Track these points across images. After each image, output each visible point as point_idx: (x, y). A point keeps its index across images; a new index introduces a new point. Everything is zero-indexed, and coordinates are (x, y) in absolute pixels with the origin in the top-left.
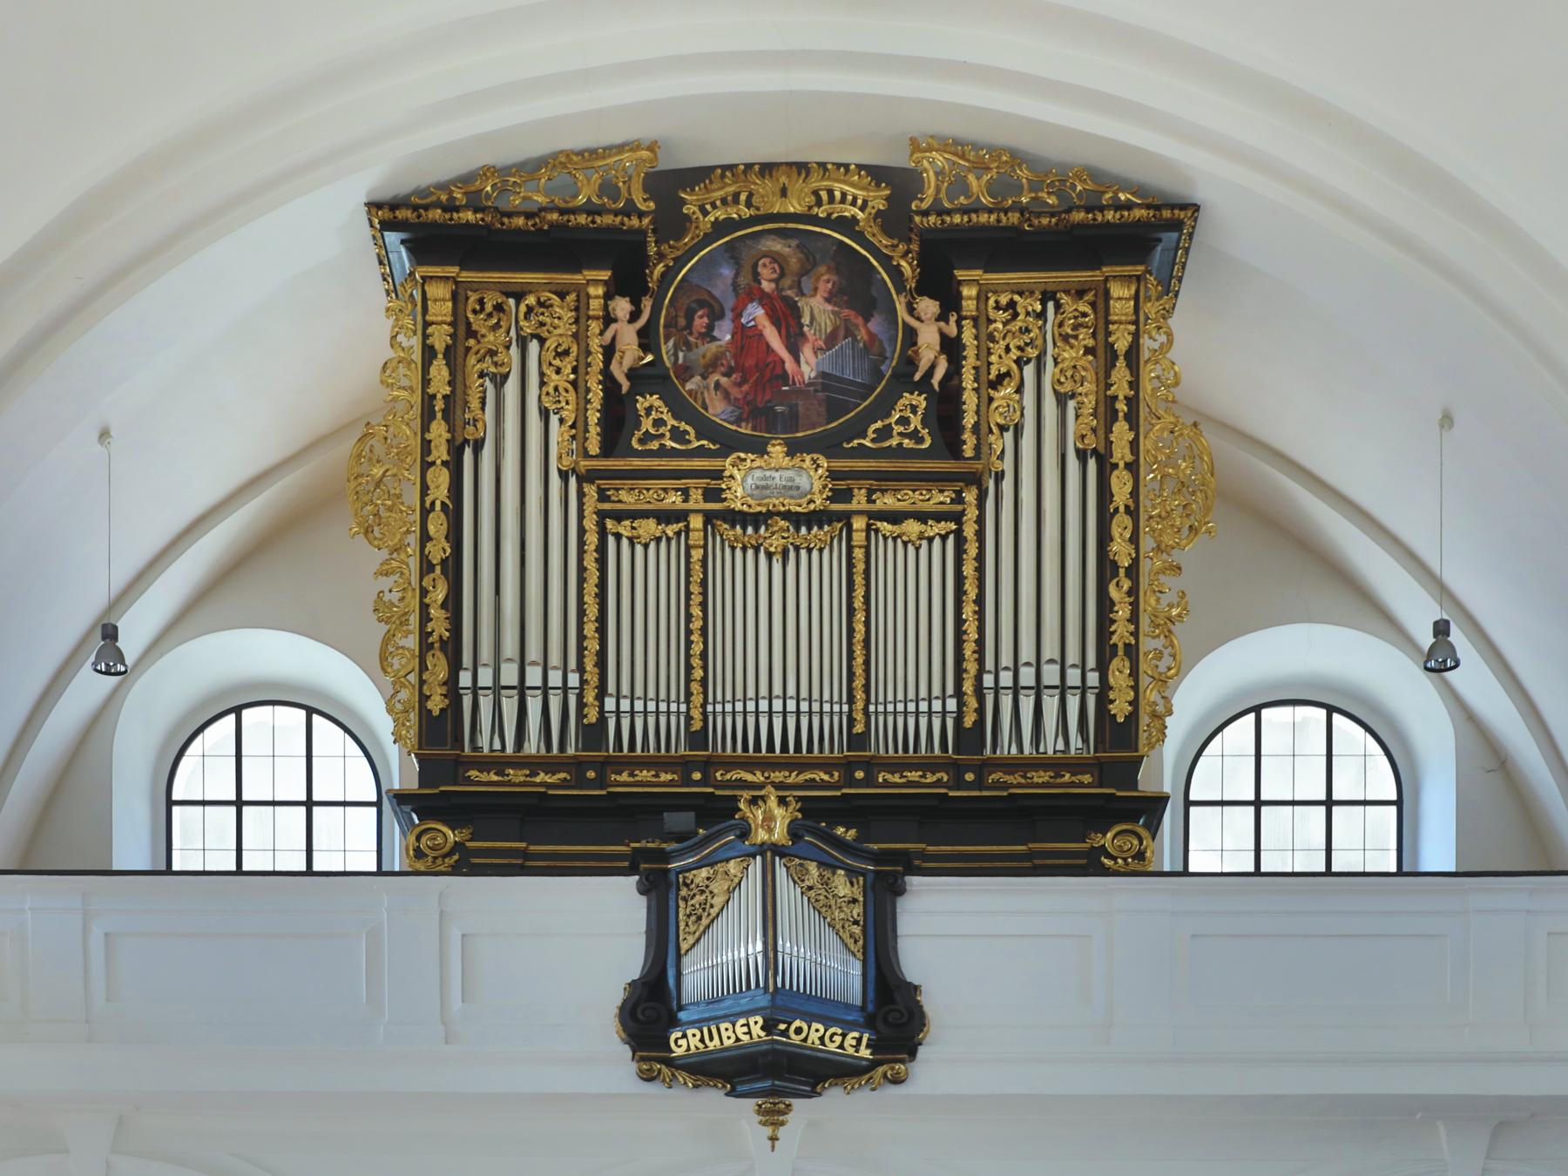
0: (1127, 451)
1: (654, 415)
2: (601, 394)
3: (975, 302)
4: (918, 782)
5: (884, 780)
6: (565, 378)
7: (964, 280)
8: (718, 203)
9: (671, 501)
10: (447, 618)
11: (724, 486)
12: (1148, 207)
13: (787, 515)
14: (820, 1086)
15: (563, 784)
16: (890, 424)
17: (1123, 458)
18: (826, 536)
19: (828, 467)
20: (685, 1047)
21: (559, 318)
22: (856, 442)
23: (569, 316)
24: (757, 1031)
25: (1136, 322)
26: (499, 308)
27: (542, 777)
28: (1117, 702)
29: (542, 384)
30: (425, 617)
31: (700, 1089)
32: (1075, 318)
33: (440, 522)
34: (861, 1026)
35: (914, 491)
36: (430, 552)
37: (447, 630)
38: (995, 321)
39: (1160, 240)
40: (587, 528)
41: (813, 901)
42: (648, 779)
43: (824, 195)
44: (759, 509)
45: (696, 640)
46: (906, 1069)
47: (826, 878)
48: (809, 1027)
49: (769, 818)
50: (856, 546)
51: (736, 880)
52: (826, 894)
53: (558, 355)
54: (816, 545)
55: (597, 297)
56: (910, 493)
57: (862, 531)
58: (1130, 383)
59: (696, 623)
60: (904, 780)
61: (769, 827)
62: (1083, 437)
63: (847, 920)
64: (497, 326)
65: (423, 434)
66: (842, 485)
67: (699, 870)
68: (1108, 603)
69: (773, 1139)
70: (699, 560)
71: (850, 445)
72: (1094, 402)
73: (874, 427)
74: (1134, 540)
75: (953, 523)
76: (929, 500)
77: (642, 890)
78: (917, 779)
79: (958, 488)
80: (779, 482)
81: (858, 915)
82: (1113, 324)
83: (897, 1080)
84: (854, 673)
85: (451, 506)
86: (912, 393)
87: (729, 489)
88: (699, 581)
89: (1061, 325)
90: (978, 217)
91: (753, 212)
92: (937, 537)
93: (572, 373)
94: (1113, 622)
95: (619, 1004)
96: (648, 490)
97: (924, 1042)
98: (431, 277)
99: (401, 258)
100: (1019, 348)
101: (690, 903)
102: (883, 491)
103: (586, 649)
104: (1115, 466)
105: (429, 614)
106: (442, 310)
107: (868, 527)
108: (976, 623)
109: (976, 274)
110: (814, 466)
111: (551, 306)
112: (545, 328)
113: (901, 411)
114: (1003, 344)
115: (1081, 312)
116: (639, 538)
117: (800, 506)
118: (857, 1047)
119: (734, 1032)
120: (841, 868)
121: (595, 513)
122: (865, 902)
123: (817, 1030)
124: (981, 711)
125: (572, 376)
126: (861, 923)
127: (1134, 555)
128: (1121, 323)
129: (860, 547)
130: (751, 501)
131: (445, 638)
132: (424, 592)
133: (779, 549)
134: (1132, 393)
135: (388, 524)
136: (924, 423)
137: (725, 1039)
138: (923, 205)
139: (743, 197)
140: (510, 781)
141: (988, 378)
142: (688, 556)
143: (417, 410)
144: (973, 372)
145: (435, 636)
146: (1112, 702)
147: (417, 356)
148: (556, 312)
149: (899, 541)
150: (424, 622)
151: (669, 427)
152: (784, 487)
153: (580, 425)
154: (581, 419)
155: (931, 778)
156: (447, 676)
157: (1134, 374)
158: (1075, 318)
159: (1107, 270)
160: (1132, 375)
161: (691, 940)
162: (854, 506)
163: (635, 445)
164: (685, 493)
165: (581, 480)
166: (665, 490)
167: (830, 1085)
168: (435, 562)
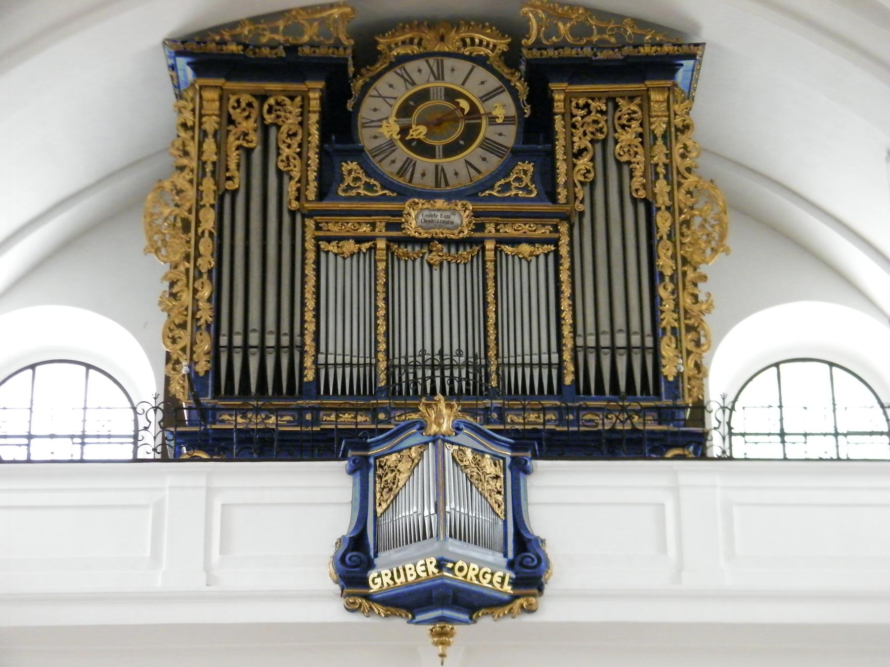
0: (666, 198)
1: (353, 175)
2: (317, 160)
3: (563, 104)
5: (512, 421)
7: (555, 90)
8: (400, 44)
10: (211, 309)
11: (403, 220)
13: (442, 241)
17: (664, 203)
18: (468, 255)
19: (473, 208)
20: (379, 585)
21: (290, 113)
24: (432, 569)
25: (669, 116)
26: (250, 105)
28: (668, 367)
29: (279, 154)
31: (389, 617)
32: (629, 114)
37: (210, 317)
38: (576, 116)
39: (682, 65)
40: (307, 248)
41: (469, 476)
42: (349, 420)
43: (468, 41)
44: (425, 236)
45: (381, 323)
46: (537, 602)
48: (468, 567)
49: (439, 415)
50: (488, 260)
51: (416, 461)
53: (289, 136)
55: (315, 99)
56: (523, 225)
58: (667, 155)
59: (381, 312)
61: (439, 423)
62: (637, 190)
66: (480, 220)
67: (390, 456)
69: (442, 656)
71: (483, 195)
72: (643, 168)
73: (499, 183)
74: (674, 257)
75: (552, 246)
76: (535, 231)
77: (351, 472)
81: (501, 487)
84: (489, 346)
86: (524, 162)
89: (620, 118)
91: (422, 50)
92: (542, 254)
94: (662, 312)
96: (348, 223)
98: (206, 86)
100: (592, 133)
101: (384, 479)
103: (306, 329)
105: (198, 306)
106: (213, 107)
107: (496, 249)
109: (564, 85)
111: (285, 105)
112: (281, 119)
113: (517, 173)
114: (582, 130)
115: (632, 111)
116: (343, 254)
118: (502, 583)
119: (416, 571)
120: (488, 453)
121: (313, 238)
122: (505, 479)
123: (474, 569)
124: (576, 373)
125: (298, 150)
126: (503, 493)
127: (674, 268)
128: (658, 116)
129: (491, 261)
130: (421, 231)
131: (209, 322)
132: (195, 291)
134: (668, 161)
135: (171, 247)
136: (533, 180)
138: (529, 41)
139: (416, 41)
141: (572, 152)
142: (376, 267)
145: (202, 321)
146: (664, 366)
151: (363, 182)
152: (443, 222)
153: (304, 180)
154: (304, 176)
158: (629, 114)
159: (648, 83)
161: (384, 506)
162: (486, 234)
164: (373, 225)
165: (304, 216)
166: (359, 223)
167: (483, 614)
168: (203, 271)
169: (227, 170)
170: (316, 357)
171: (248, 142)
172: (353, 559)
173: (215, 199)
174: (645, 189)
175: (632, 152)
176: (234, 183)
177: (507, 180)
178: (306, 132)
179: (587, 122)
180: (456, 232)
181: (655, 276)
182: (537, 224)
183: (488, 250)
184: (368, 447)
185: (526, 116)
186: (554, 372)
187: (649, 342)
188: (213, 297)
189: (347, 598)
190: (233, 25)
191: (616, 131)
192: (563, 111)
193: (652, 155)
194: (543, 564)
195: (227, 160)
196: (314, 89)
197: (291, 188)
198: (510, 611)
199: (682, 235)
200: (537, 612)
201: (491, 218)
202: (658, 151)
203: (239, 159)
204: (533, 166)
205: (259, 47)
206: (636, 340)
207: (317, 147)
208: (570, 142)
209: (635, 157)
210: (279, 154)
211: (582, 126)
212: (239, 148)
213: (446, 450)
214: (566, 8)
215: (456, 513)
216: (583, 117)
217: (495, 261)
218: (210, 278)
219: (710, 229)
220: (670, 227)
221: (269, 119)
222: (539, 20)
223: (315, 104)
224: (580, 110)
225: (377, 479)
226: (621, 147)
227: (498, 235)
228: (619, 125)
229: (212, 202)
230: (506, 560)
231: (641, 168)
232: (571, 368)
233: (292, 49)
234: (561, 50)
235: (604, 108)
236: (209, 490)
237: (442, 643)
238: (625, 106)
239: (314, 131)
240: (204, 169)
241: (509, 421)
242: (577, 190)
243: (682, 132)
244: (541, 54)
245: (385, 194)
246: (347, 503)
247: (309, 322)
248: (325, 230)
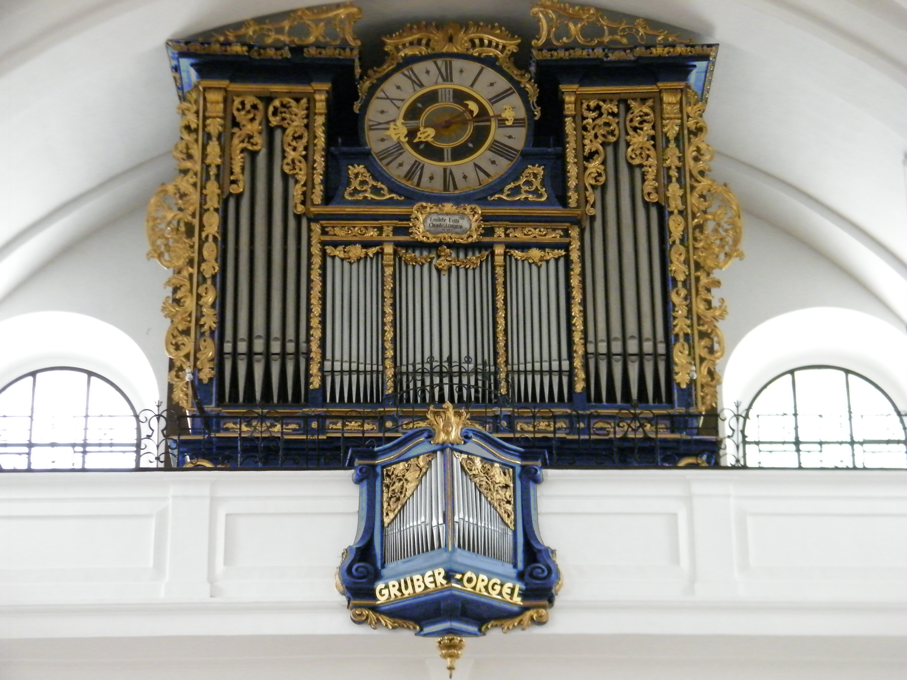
0: (679, 202)
1: (360, 178)
2: (323, 164)
3: (573, 106)
5: (522, 429)
7: (566, 92)
8: (407, 45)
10: (215, 315)
11: (411, 224)
13: (450, 246)
17: (676, 207)
18: (477, 260)
19: (482, 213)
20: (387, 596)
21: (296, 115)
24: (440, 580)
25: (682, 119)
26: (254, 107)
28: (680, 374)
29: (284, 157)
31: (397, 630)
32: (641, 116)
33: (211, 250)
37: (214, 323)
38: (587, 118)
39: (695, 66)
40: (313, 253)
41: (478, 485)
42: (356, 428)
43: (477, 41)
44: (434, 240)
45: (388, 330)
47: (487, 469)
49: (448, 424)
50: (497, 265)
51: (424, 470)
53: (295, 138)
54: (470, 266)
55: (321, 101)
56: (533, 230)
58: (679, 158)
59: (388, 318)
61: (448, 431)
62: (649, 194)
63: (502, 500)
66: (489, 224)
69: (451, 668)
70: (390, 275)
71: (493, 198)
72: (655, 171)
74: (687, 262)
75: (563, 251)
76: (545, 235)
77: (358, 481)
80: (448, 223)
81: (510, 496)
84: (498, 353)
86: (534, 165)
89: (631, 120)
91: (430, 51)
94: (675, 318)
96: (354, 227)
98: (210, 88)
100: (604, 136)
101: (391, 489)
103: (312, 335)
104: (671, 213)
105: (201, 312)
106: (217, 109)
107: (505, 254)
109: (574, 87)
110: (472, 213)
111: (290, 107)
112: (286, 122)
113: (527, 177)
114: (593, 132)
115: (644, 113)
116: (349, 259)
117: (462, 239)
118: (512, 594)
119: (423, 582)
120: (497, 462)
121: (319, 243)
122: (514, 488)
123: (483, 580)
124: (587, 380)
125: (304, 153)
126: (512, 502)
127: (687, 273)
128: (670, 119)
129: (500, 266)
130: (429, 235)
131: (213, 329)
132: (199, 297)
133: (445, 268)
134: (681, 164)
135: (175, 251)
136: (543, 184)
138: (540, 42)
139: (424, 42)
142: (383, 272)
145: (206, 327)
148: (293, 111)
149: (526, 262)
151: (370, 186)
152: (452, 226)
153: (310, 184)
154: (310, 179)
156: (214, 355)
158: (641, 116)
159: (661, 85)
161: (392, 516)
162: (495, 238)
163: (348, 197)
164: (380, 229)
165: (310, 220)
166: (366, 227)
167: (492, 626)
168: (207, 276)
169: (232, 173)
170: (322, 364)
171: (253, 144)
172: (360, 569)
173: (219, 203)
174: (657, 193)
175: (644, 155)
176: (239, 186)
177: (517, 184)
178: (312, 135)
180: (465, 236)
181: (667, 282)
182: (547, 229)
183: (498, 255)
184: (374, 456)
185: (537, 118)
186: (565, 380)
187: (661, 348)
188: (217, 303)
189: (354, 610)
190: (238, 26)
191: (627, 134)
192: (574, 113)
193: (665, 158)
194: (553, 575)
196: (320, 91)
197: (296, 192)
198: (519, 623)
199: (695, 239)
200: (547, 624)
203: (244, 162)
204: (543, 169)
206: (648, 347)
208: (581, 145)
209: (647, 160)
210: (284, 157)
211: (593, 129)
212: (243, 150)
213: (455, 459)
214: (577, 8)
215: (465, 522)
216: (594, 120)
217: (505, 266)
218: (214, 283)
219: (724, 234)
220: (683, 231)
221: (274, 121)
222: (549, 20)
223: (321, 106)
224: (591, 112)
225: (384, 488)
227: (508, 240)
228: (631, 127)
229: (216, 206)
230: (515, 571)
231: (653, 171)
232: (582, 375)
233: (297, 50)
234: (571, 51)
235: (616, 110)
236: (213, 499)
237: (451, 656)
238: (637, 109)
240: (208, 173)
241: (519, 429)
242: (588, 193)
243: (696, 135)
244: (552, 55)
245: (392, 198)
246: (354, 513)
247: (315, 329)
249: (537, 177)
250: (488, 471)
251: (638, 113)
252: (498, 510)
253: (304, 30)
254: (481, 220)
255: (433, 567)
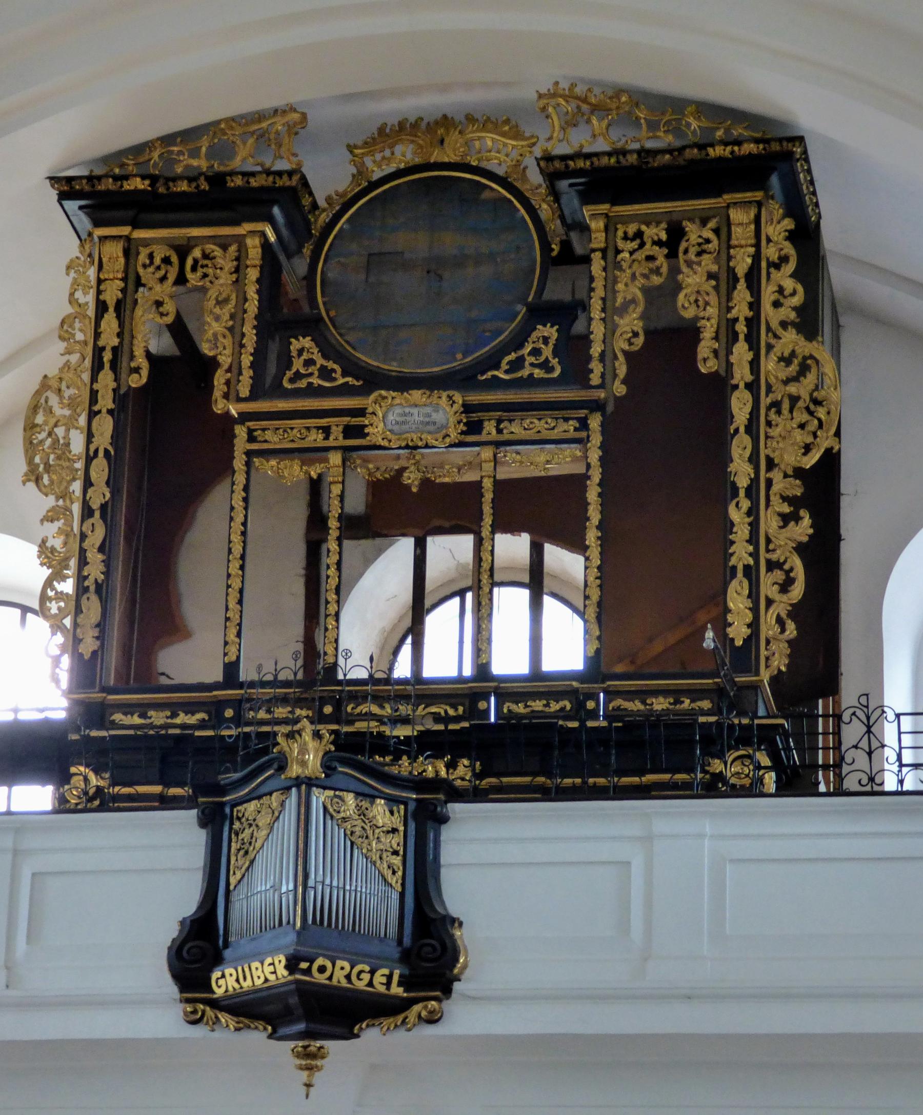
1: (305, 356)
2: (255, 338)
3: (604, 234)
4: (542, 711)
5: (509, 711)
6: (224, 324)
9: (312, 439)
11: (367, 422)
12: (757, 141)
14: (357, 1027)
15: (202, 725)
16: (523, 355)
17: (742, 378)
20: (223, 989)
21: (221, 269)
22: (490, 374)
23: (230, 265)
24: (282, 972)
26: (166, 261)
27: (182, 718)
30: (83, 562)
31: (242, 1031)
32: (699, 244)
34: (393, 961)
35: (540, 419)
36: (90, 498)
37: (102, 573)
38: (622, 251)
41: (349, 833)
47: (363, 808)
49: (303, 750)
52: (363, 824)
53: (218, 303)
56: (536, 421)
57: (490, 461)
60: (528, 710)
63: (386, 850)
64: (163, 279)
65: (92, 384)
66: (475, 416)
68: (729, 524)
69: (308, 1085)
72: (715, 326)
74: (754, 459)
76: (553, 428)
77: (203, 824)
78: (540, 709)
79: (583, 416)
81: (398, 845)
82: (734, 248)
83: (433, 1019)
85: (112, 453)
86: (545, 326)
87: (372, 425)
88: (337, 516)
90: (714, 150)
93: (230, 320)
94: (732, 543)
95: (169, 944)
96: (292, 429)
97: (463, 977)
98: (106, 237)
99: (83, 222)
102: (510, 421)
104: (736, 387)
105: (86, 558)
108: (599, 549)
111: (214, 258)
113: (534, 342)
118: (388, 985)
119: (263, 971)
120: (381, 798)
123: (342, 968)
126: (401, 853)
127: (753, 476)
128: (742, 247)
131: (100, 581)
136: (555, 353)
137: (255, 979)
140: (152, 723)
143: (88, 363)
144: (600, 302)
145: (91, 579)
147: (91, 312)
150: (82, 565)
151: (318, 366)
152: (422, 423)
155: (555, 707)
157: (755, 295)
159: (727, 197)
160: (752, 296)
161: (239, 875)
162: (483, 437)
163: (287, 385)
164: (326, 431)
167: (368, 1026)
169: (132, 357)
172: (194, 950)
173: (114, 402)
176: (140, 376)
178: (241, 297)
179: (637, 260)
182: (557, 419)
184: (222, 790)
185: (554, 254)
190: (138, 150)
192: (602, 245)
193: (730, 304)
195: (132, 344)
199: (769, 424)
201: (491, 414)
202: (738, 298)
204: (557, 330)
205: (174, 180)
207: (256, 318)
211: (630, 267)
213: (314, 799)
215: (325, 887)
218: (103, 516)
220: (751, 414)
224: (628, 242)
225: (233, 836)
226: (686, 295)
228: (685, 261)
230: (400, 949)
231: (712, 326)
233: (218, 180)
234: (595, 160)
236: (16, 852)
237: (309, 1068)
238: (694, 233)
239: (252, 294)
240: (101, 358)
242: (617, 364)
243: (777, 267)
245: (347, 382)
246: (198, 869)
248: (260, 442)
249: (548, 343)
250: (366, 812)
251: (694, 240)
252: (378, 865)
253: (222, 151)
254: (462, 413)
255: (273, 952)
